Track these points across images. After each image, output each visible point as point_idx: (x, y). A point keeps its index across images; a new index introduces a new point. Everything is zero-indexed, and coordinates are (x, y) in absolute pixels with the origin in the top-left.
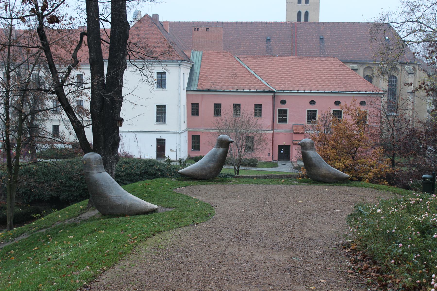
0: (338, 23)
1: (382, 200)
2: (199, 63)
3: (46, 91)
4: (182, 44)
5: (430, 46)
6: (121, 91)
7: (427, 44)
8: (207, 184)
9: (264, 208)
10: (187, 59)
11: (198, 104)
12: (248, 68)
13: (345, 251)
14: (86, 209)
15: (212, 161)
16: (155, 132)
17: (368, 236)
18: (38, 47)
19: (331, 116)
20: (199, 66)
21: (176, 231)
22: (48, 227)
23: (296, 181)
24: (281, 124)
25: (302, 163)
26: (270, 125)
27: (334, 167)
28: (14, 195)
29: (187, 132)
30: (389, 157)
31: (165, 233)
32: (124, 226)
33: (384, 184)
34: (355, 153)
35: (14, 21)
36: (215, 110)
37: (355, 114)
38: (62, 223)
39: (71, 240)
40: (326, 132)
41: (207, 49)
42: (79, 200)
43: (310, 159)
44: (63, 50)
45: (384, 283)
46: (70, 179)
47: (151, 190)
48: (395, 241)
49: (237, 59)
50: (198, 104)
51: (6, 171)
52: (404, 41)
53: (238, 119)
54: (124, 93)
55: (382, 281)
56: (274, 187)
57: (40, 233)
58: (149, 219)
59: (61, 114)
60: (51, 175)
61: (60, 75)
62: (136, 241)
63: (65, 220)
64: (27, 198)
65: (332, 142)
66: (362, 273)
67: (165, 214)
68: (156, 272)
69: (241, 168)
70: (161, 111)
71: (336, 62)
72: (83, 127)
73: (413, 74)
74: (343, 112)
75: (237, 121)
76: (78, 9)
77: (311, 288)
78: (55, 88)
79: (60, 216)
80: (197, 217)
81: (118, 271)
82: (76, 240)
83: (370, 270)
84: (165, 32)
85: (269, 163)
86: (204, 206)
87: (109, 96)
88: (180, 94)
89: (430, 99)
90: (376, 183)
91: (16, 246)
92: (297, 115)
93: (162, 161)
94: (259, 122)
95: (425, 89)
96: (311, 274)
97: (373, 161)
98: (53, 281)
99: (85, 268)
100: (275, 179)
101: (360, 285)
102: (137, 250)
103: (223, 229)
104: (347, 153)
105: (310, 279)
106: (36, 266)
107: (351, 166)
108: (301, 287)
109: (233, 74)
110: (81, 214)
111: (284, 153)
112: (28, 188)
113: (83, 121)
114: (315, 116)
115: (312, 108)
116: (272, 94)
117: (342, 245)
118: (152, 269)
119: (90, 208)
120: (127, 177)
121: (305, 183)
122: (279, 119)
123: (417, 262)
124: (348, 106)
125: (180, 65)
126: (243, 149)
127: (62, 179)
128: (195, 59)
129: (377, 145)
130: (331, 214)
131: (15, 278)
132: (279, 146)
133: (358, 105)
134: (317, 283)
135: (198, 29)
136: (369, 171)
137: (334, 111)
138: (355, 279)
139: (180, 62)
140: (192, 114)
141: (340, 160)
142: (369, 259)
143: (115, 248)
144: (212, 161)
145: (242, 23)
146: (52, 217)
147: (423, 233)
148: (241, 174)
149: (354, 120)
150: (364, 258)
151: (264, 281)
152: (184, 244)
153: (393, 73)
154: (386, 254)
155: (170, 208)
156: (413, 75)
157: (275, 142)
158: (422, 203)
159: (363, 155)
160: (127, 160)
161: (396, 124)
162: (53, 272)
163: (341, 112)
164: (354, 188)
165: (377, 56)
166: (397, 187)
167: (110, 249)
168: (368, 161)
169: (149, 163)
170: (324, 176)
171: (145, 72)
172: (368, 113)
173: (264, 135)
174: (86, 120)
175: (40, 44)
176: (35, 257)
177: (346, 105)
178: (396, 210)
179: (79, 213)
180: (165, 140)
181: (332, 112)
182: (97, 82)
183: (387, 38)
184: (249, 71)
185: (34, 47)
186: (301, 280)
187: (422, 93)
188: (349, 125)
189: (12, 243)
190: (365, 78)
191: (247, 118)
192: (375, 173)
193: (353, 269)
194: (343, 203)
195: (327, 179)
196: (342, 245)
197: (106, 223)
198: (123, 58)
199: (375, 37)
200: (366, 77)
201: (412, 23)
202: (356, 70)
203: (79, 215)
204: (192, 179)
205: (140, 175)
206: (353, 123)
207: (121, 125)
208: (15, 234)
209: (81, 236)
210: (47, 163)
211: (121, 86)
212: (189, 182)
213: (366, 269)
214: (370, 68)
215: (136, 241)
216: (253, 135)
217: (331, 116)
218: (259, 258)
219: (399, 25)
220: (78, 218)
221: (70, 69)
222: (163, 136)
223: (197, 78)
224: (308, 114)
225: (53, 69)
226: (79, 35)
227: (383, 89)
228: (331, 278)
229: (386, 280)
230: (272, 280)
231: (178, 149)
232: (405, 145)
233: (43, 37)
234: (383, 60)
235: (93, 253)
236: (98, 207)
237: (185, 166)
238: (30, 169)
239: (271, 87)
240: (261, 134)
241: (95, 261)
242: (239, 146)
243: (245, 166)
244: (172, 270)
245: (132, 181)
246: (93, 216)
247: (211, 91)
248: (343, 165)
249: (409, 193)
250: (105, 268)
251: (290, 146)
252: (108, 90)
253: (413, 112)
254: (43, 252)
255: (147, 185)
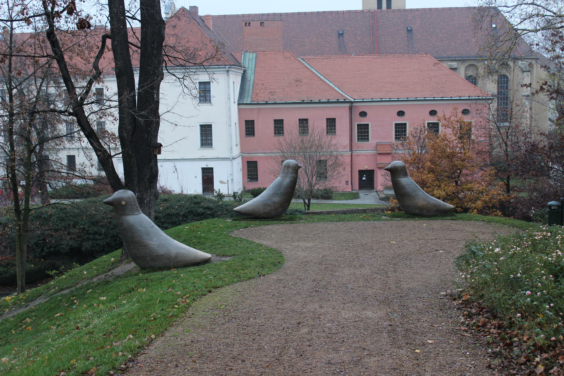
0: (430, 9)
1: (499, 236)
2: (253, 68)
3: (61, 112)
4: (230, 44)
5: (553, 35)
6: (157, 108)
7: (549, 33)
8: (272, 224)
9: (347, 252)
10: (237, 64)
11: (253, 121)
12: (316, 72)
13: (455, 303)
14: (119, 262)
15: (277, 194)
16: (200, 159)
17: (486, 283)
18: (48, 56)
19: (425, 130)
20: (253, 72)
21: (238, 286)
22: (71, 287)
23: (385, 216)
24: (362, 143)
25: (392, 192)
26: (347, 145)
27: (433, 195)
28: (25, 249)
29: (240, 158)
30: (502, 180)
31: (223, 289)
32: (170, 282)
33: (496, 215)
34: (459, 176)
35: (15, 24)
36: (275, 127)
37: (456, 127)
38: (89, 281)
39: (103, 303)
40: (420, 151)
41: (262, 49)
42: (106, 250)
43: (403, 187)
44: (79, 58)
45: (508, 341)
46: (95, 223)
47: (201, 234)
48: (520, 287)
49: (301, 60)
50: (253, 121)
51: (12, 215)
52: (517, 30)
53: (306, 138)
54: (161, 111)
55: (506, 339)
56: (358, 225)
57: (62, 295)
58: (202, 271)
59: (80, 141)
60: (69, 219)
61: (78, 91)
62: (188, 301)
63: (92, 278)
64: (40, 250)
65: (429, 164)
66: (479, 330)
67: (221, 265)
68: (218, 339)
69: (312, 201)
70: (206, 131)
71: (430, 60)
72: (110, 157)
73: (529, 71)
74: (440, 124)
75: (304, 141)
76: (98, 5)
77: (417, 351)
78: (73, 109)
79: (85, 273)
80: (262, 267)
81: (170, 340)
82: (110, 302)
83: (489, 326)
84: (207, 29)
85: (348, 194)
86: (271, 252)
87: (142, 116)
88: (230, 109)
89: (552, 104)
90: (486, 214)
91: (32, 312)
92: (382, 130)
93: (209, 196)
94: (334, 142)
95: (548, 91)
96: (416, 333)
97: (483, 186)
98: (88, 355)
99: (128, 337)
100: (358, 215)
101: (478, 345)
102: (190, 311)
103: (298, 280)
104: (448, 177)
105: (415, 341)
106: (62, 337)
107: (454, 193)
108: (404, 351)
109: (297, 81)
110: (114, 268)
111: (367, 180)
112: (41, 238)
113: (109, 148)
114: (405, 131)
115: (400, 121)
116: (348, 105)
117: (451, 296)
118: (213, 336)
119: (123, 260)
120: (167, 219)
121: (398, 217)
122: (358, 136)
123: (551, 314)
124: (447, 117)
125: (228, 71)
126: (314, 177)
127: (83, 225)
128: (247, 63)
129: (486, 165)
130: (435, 255)
131: (37, 354)
132: (359, 171)
133: (460, 115)
134: (424, 345)
135: (249, 23)
136: (478, 199)
137: (429, 124)
138: (471, 338)
139: (229, 68)
140: (246, 134)
141: (439, 186)
142: (487, 312)
143: (163, 310)
144: (277, 194)
145: (305, 13)
146: (75, 274)
147: (556, 276)
148: (312, 209)
149: (456, 134)
150: (481, 311)
151: (356, 345)
152: (249, 302)
153: (504, 72)
154: (510, 305)
155: (227, 256)
156: (529, 73)
157: (354, 167)
158: (550, 239)
159: (469, 178)
160: (166, 197)
161: (510, 137)
162: (86, 344)
163: (437, 124)
164: (461, 222)
165: (483, 50)
166: (514, 218)
167: (156, 312)
168: (476, 187)
169: (194, 199)
170: (421, 208)
171: (186, 83)
172: (473, 124)
173: (340, 158)
174: (115, 149)
175: (50, 51)
176: (59, 325)
177: (444, 115)
178: (518, 249)
179: (110, 268)
180: (212, 169)
181: (426, 125)
182: (127, 99)
183: (494, 26)
184: (317, 76)
185: (44, 57)
186: (402, 342)
187: (543, 97)
188: (449, 142)
189: (27, 308)
190: (467, 79)
191: (318, 137)
192: (485, 202)
193: (467, 325)
194: (447, 241)
195: (425, 211)
196: (451, 296)
197: (146, 279)
198: (159, 66)
199: (480, 27)
200: (469, 78)
201: (526, 6)
202: (455, 69)
203: (110, 270)
204: (252, 218)
205: (184, 216)
206: (455, 138)
207: (159, 153)
208: (28, 297)
209: (115, 297)
210: (63, 204)
211: (158, 102)
212: (249, 222)
213: (484, 325)
214: (472, 66)
215: (188, 301)
216: (326, 158)
217: (425, 130)
218: (346, 316)
219: (510, 9)
220: (110, 273)
221: (90, 83)
222: (210, 165)
223: (251, 87)
224: (396, 128)
225: (69, 83)
226: (99, 39)
227: (491, 93)
228: (441, 338)
229: (510, 338)
230: (366, 344)
231: (229, 180)
232: (523, 163)
233: (54, 44)
234: (491, 56)
235: (136, 318)
236: (135, 259)
237: (240, 202)
238: (42, 213)
239: (346, 96)
240: (336, 157)
241: (139, 327)
242: (309, 173)
243: (318, 198)
244: (238, 336)
245: (175, 224)
246: (129, 271)
247: (269, 104)
248: (444, 193)
249: (531, 226)
250: (153, 336)
251: (374, 170)
252: (141, 108)
253: (531, 121)
254: (69, 319)
255: (195, 228)
